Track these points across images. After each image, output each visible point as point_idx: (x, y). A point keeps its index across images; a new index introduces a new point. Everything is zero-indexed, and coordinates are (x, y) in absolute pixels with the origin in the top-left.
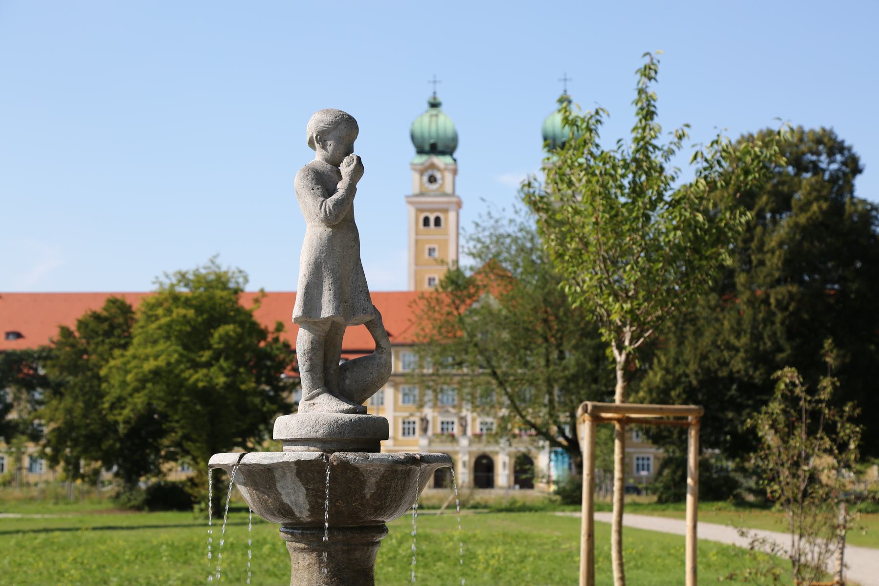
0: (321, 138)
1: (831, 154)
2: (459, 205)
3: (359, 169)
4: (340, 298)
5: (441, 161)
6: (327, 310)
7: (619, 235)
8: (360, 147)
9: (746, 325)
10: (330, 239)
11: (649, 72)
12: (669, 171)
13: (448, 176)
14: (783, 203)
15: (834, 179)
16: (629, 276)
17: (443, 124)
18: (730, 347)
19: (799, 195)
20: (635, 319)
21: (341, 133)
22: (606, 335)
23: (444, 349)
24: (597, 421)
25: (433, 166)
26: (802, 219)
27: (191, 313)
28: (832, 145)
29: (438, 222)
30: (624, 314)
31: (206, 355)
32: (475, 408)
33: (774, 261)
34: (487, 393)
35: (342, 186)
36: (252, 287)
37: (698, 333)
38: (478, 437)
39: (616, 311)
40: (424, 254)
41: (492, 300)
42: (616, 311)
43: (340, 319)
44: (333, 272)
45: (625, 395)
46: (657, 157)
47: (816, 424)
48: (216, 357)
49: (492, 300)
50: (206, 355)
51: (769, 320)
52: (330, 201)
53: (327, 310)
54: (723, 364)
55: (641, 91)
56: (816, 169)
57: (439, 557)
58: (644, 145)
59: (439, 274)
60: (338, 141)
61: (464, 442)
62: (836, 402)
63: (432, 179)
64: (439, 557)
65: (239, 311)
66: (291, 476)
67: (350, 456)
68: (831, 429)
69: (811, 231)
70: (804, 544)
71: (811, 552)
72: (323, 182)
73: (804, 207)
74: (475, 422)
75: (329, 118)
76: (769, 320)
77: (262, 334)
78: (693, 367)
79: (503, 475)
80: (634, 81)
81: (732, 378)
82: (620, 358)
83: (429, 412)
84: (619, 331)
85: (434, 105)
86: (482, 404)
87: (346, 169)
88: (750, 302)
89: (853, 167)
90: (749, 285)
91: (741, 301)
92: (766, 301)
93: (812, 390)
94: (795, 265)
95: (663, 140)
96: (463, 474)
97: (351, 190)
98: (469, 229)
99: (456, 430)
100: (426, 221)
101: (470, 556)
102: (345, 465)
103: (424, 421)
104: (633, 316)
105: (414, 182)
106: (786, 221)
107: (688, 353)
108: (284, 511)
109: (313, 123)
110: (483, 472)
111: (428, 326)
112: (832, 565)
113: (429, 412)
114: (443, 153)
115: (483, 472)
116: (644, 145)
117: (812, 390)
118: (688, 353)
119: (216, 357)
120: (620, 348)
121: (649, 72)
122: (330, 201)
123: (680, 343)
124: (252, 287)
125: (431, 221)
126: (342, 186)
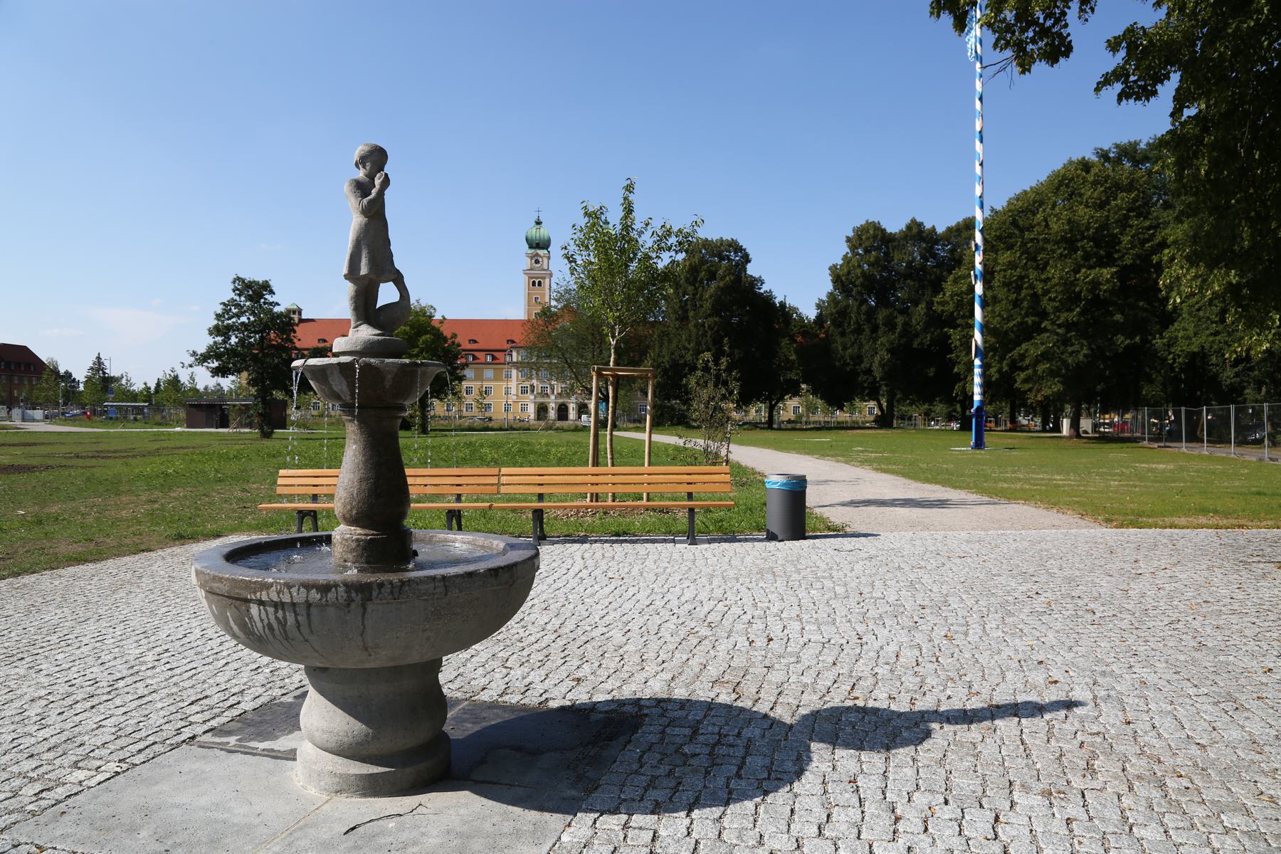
0: (362, 161)
1: (736, 253)
2: (551, 275)
3: (386, 183)
4: (372, 263)
5: (541, 252)
6: (364, 270)
7: (613, 276)
8: (388, 169)
9: (693, 338)
10: (366, 225)
11: (629, 188)
12: (640, 241)
13: (545, 260)
14: (712, 276)
15: (737, 264)
16: (618, 297)
17: (544, 232)
18: (685, 348)
19: (720, 272)
20: (621, 321)
21: (376, 158)
22: (606, 330)
23: (540, 349)
24: (599, 375)
25: (537, 255)
26: (721, 284)
27: (408, 328)
28: (735, 246)
29: (540, 284)
30: (615, 319)
31: (416, 351)
32: (557, 379)
33: (707, 305)
34: (563, 372)
35: (374, 192)
36: (438, 316)
37: (670, 341)
38: (560, 395)
39: (611, 317)
40: (532, 300)
41: (566, 322)
42: (611, 317)
43: (373, 277)
44: (369, 246)
45: (616, 363)
46: (634, 234)
47: (719, 382)
48: (422, 351)
49: (566, 322)
50: (416, 351)
51: (704, 335)
52: (365, 201)
53: (364, 270)
54: (682, 357)
55: (625, 199)
56: (729, 259)
57: (532, 452)
58: (627, 228)
59: (538, 309)
60: (373, 163)
61: (553, 397)
62: (729, 370)
63: (537, 262)
64: (532, 452)
65: (433, 328)
66: (336, 373)
67: (372, 360)
68: (725, 383)
69: (725, 290)
70: (710, 442)
71: (713, 446)
72: (362, 188)
73: (723, 278)
74: (558, 387)
75: (367, 148)
76: (704, 335)
77: (445, 340)
78: (667, 358)
79: (572, 414)
80: (621, 193)
81: (686, 364)
82: (613, 343)
83: (535, 382)
84: (613, 328)
85: (538, 223)
86: (560, 378)
87: (377, 182)
88: (696, 326)
89: (747, 259)
90: (695, 317)
91: (691, 326)
92: (703, 325)
93: (717, 363)
94: (719, 307)
95: (638, 225)
96: (552, 414)
97: (381, 194)
98: (554, 286)
99: (549, 391)
100: (534, 283)
101: (548, 452)
102: (369, 365)
103: (532, 386)
104: (620, 320)
105: (527, 263)
106: (714, 285)
107: (665, 352)
108: (336, 396)
109: (359, 150)
110: (562, 412)
111: (532, 336)
112: (723, 452)
113: (535, 382)
114: (543, 248)
115: (562, 412)
116: (627, 228)
117: (717, 363)
118: (665, 352)
119: (422, 351)
120: (613, 337)
121: (629, 188)
122: (365, 201)
123: (661, 346)
124: (438, 316)
125: (536, 283)
126: (374, 192)
